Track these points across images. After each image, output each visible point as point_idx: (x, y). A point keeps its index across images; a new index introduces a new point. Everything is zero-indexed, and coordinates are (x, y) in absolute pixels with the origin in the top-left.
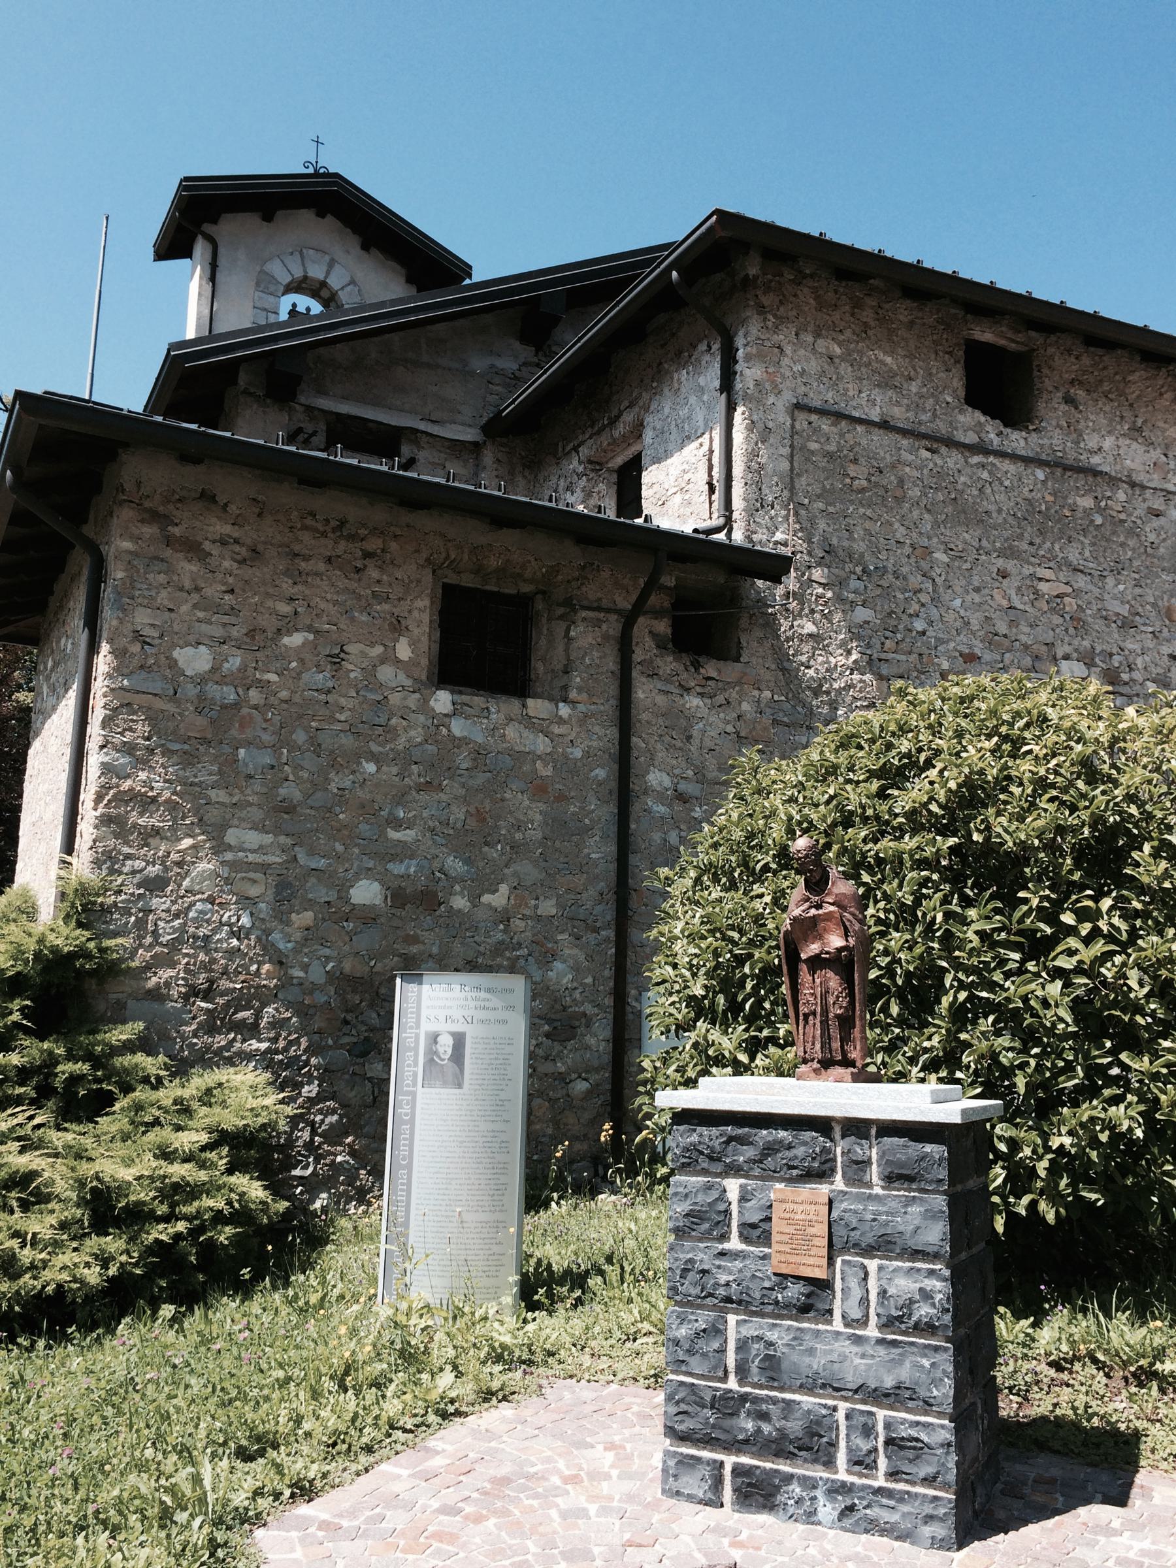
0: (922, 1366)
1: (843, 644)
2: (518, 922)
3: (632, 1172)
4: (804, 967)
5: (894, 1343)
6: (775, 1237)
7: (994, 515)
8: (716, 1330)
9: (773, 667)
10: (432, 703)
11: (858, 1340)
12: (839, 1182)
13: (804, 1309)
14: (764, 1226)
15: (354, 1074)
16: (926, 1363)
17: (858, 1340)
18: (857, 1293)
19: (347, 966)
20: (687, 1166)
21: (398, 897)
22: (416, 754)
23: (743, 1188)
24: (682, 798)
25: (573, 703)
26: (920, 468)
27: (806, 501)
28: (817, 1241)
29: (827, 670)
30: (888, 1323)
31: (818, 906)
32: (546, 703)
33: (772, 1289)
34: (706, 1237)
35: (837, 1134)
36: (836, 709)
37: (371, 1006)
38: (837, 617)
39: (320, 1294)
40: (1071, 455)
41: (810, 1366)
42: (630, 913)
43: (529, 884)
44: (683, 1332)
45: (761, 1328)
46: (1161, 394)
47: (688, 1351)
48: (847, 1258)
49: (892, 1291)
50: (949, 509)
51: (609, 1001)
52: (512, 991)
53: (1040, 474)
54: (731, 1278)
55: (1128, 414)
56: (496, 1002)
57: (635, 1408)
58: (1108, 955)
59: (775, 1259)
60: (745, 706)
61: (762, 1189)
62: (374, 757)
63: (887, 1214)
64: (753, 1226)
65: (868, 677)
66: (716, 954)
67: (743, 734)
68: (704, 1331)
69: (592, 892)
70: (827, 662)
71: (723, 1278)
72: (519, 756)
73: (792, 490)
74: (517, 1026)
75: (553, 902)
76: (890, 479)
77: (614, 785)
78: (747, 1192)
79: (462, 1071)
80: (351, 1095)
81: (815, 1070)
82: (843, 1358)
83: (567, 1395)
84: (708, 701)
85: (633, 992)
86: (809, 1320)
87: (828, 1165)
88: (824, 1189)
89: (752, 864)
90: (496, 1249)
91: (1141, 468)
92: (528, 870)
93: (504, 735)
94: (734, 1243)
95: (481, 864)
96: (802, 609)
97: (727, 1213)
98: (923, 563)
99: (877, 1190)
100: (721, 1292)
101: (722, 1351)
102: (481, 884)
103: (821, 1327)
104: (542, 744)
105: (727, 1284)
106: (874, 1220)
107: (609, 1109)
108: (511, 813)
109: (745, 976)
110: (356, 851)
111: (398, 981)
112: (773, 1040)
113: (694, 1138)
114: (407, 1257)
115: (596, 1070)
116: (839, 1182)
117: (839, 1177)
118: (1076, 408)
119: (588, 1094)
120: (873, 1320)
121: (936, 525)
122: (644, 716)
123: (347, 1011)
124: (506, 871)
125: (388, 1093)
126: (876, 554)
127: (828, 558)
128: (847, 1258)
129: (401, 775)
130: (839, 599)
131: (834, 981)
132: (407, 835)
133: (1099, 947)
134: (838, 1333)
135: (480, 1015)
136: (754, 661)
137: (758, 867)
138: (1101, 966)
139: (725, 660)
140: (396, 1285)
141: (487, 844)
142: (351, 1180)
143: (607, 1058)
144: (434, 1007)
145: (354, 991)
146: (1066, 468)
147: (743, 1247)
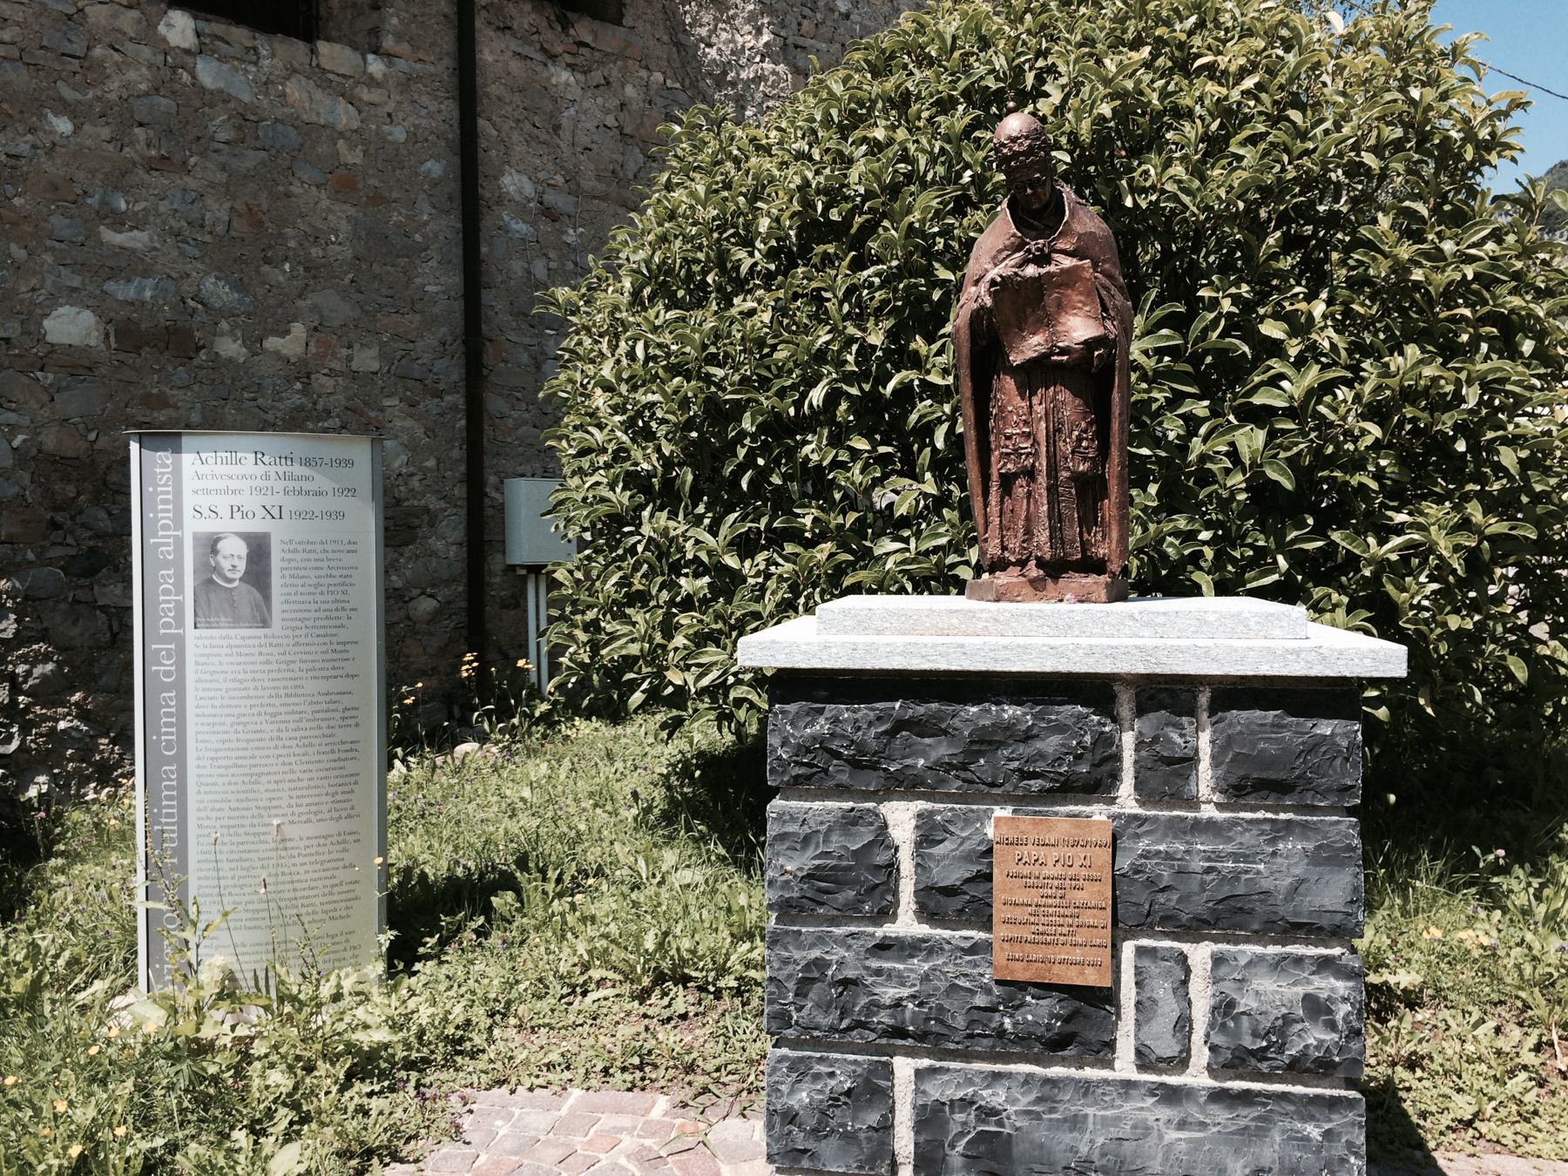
0: (1307, 1139)
1: (751, 18)
2: (323, 380)
3: (505, 713)
4: (1009, 383)
5: (1246, 1097)
6: (999, 913)
8: (873, 1090)
9: (666, 38)
10: (162, 29)
11: (1171, 1095)
12: (1126, 797)
13: (1055, 1045)
14: (976, 891)
15: (76, 601)
16: (1313, 1132)
17: (1171, 1095)
18: (1169, 1009)
19: (50, 440)
20: (806, 784)
21: (127, 334)
22: (141, 109)
23: (924, 818)
24: (550, 214)
25: (389, 56)
28: (1088, 917)
29: (733, 53)
30: (1233, 1061)
31: (1042, 259)
32: (348, 51)
33: (992, 1009)
34: (848, 913)
35: (1125, 709)
36: (744, 108)
37: (96, 500)
39: (28, 976)
41: (1073, 1150)
42: (485, 372)
43: (336, 323)
44: (802, 1097)
45: (970, 1082)
47: (814, 1131)
48: (1145, 942)
49: (1246, 1002)
51: (460, 491)
52: (349, 463)
54: (905, 992)
56: (321, 481)
57: (628, 1143)
58: (1327, 387)
59: (1000, 955)
60: (630, 91)
61: (967, 822)
62: (65, 108)
63: (1236, 857)
64: (950, 892)
65: (781, 68)
67: (626, 131)
68: (848, 1093)
69: (430, 341)
70: (733, 41)
71: (889, 993)
72: (310, 130)
74: (363, 523)
75: (374, 352)
77: (454, 186)
78: (935, 826)
79: (267, 597)
80: (75, 633)
81: (1033, 583)
82: (1143, 1130)
83: (503, 1128)
84: (581, 77)
85: (492, 479)
86: (1064, 1062)
87: (1106, 768)
88: (1098, 813)
90: (342, 875)
92: (333, 303)
93: (283, 95)
94: (906, 924)
95: (260, 291)
97: (892, 868)
99: (1208, 812)
100: (884, 1018)
101: (886, 1127)
102: (263, 321)
103: (1090, 1073)
104: (345, 116)
105: (898, 1004)
106: (1209, 870)
107: (465, 632)
108: (302, 216)
110: (48, 258)
111: (134, 447)
112: (795, 535)
113: (821, 726)
114: (186, 920)
115: (448, 582)
116: (1126, 797)
117: (1126, 788)
119: (436, 616)
120: (1201, 1055)
122: (494, 89)
123: (55, 509)
124: (300, 303)
125: (131, 628)
128: (1145, 942)
129: (119, 141)
131: (1068, 404)
132: (135, 239)
133: (1312, 375)
134: (1128, 1085)
135: (293, 503)
136: (639, 25)
138: (1319, 402)
139: (603, 20)
140: (171, 962)
141: (267, 261)
142: (85, 754)
143: (459, 568)
144: (207, 492)
145: (66, 478)
147: (924, 930)
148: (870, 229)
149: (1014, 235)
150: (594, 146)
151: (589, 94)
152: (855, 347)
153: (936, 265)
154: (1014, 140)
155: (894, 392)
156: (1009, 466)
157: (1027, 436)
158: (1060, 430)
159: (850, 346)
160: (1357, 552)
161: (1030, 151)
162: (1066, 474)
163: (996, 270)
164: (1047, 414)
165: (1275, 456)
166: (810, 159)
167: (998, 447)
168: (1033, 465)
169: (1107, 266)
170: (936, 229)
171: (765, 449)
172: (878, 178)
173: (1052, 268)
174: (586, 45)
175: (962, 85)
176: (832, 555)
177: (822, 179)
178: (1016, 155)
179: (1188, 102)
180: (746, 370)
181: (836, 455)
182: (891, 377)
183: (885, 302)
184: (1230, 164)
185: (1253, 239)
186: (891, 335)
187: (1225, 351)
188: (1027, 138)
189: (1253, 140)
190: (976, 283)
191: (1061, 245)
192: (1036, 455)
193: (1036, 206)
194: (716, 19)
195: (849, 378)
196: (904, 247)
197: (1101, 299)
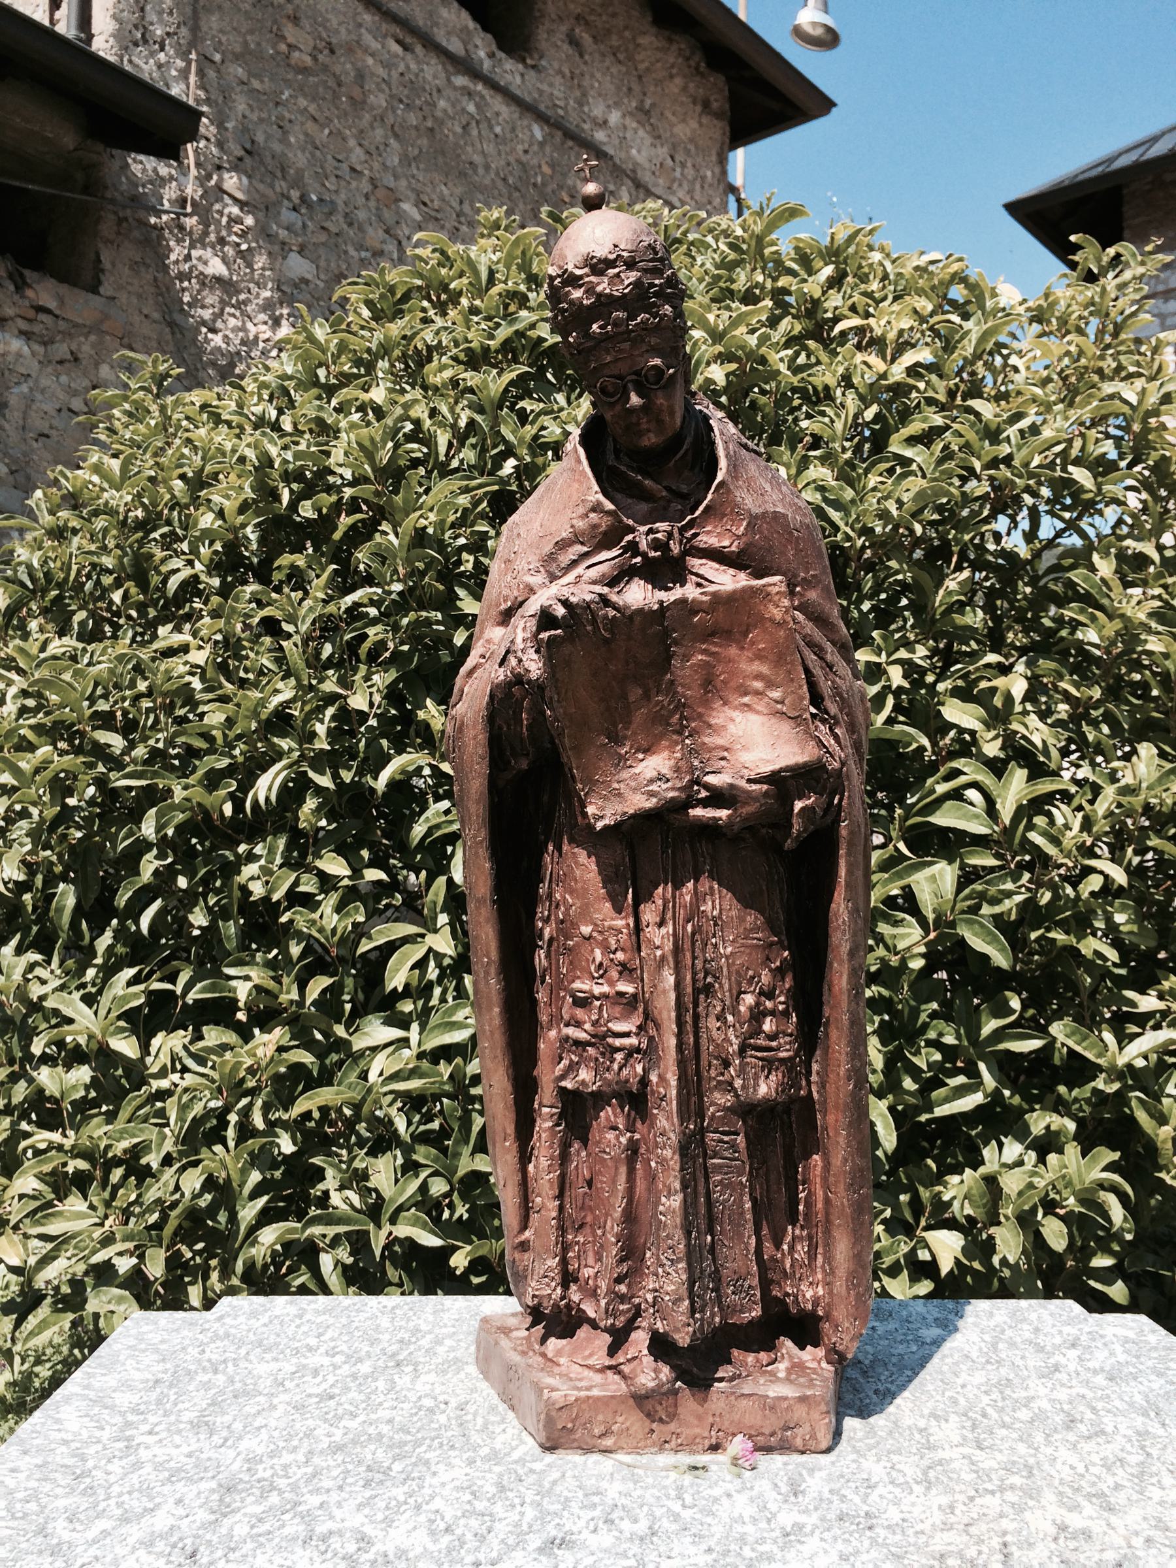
1: (267, 306)
4: (584, 867)
7: (481, 171)
9: (156, 315)
26: (388, 66)
27: (217, 57)
29: (243, 342)
38: (260, 261)
40: (573, 120)
46: (671, 77)
50: (424, 142)
53: (538, 132)
55: (636, 88)
66: (61, 787)
70: (243, 329)
73: (195, 29)
76: (345, 67)
84: (40, 349)
89: (155, 580)
91: (647, 165)
96: (206, 233)
98: (387, 214)
109: (142, 847)
112: (219, 1011)
118: (581, 56)
121: (406, 160)
126: (322, 177)
127: (248, 160)
130: (263, 232)
131: (726, 919)
136: (123, 297)
137: (173, 583)
138: (1030, 827)
146: (569, 135)
148: (361, 534)
149: (596, 508)
150: (53, 433)
151: (50, 369)
152: (330, 711)
153: (461, 593)
154: (598, 266)
155: (392, 784)
156: (584, 1074)
157: (630, 1003)
158: (708, 990)
159: (320, 710)
160: (1089, 1055)
161: (638, 299)
162: (724, 1099)
163: (555, 589)
164: (677, 950)
165: (975, 910)
166: (276, 427)
167: (556, 1019)
168: (644, 1081)
169: (812, 595)
170: (462, 541)
171: (187, 859)
172: (370, 456)
173: (690, 591)
174: (48, 311)
175: (503, 333)
176: (281, 1049)
177: (289, 456)
178: (605, 304)
179: (831, 380)
180: (159, 740)
181: (296, 883)
182: (387, 759)
183: (381, 645)
184: (890, 471)
185: (927, 580)
186: (393, 695)
187: (892, 744)
188: (630, 265)
189: (925, 439)
190: (506, 617)
191: (709, 538)
192: (649, 1053)
193: (651, 440)
194: (222, 301)
195: (320, 761)
196: (408, 561)
197: (807, 671)
